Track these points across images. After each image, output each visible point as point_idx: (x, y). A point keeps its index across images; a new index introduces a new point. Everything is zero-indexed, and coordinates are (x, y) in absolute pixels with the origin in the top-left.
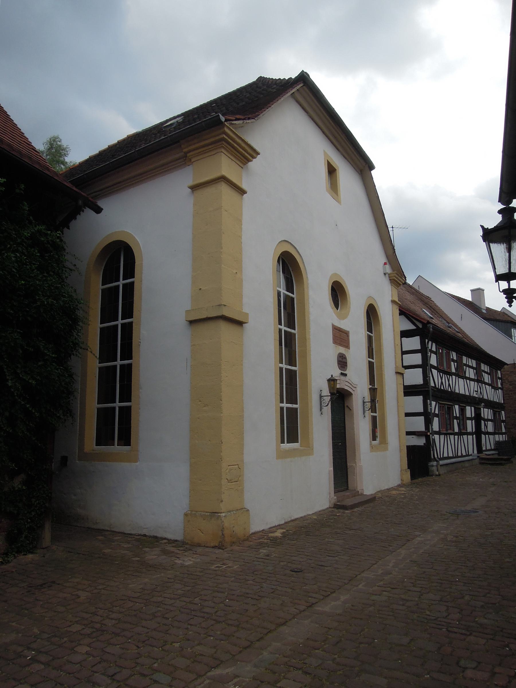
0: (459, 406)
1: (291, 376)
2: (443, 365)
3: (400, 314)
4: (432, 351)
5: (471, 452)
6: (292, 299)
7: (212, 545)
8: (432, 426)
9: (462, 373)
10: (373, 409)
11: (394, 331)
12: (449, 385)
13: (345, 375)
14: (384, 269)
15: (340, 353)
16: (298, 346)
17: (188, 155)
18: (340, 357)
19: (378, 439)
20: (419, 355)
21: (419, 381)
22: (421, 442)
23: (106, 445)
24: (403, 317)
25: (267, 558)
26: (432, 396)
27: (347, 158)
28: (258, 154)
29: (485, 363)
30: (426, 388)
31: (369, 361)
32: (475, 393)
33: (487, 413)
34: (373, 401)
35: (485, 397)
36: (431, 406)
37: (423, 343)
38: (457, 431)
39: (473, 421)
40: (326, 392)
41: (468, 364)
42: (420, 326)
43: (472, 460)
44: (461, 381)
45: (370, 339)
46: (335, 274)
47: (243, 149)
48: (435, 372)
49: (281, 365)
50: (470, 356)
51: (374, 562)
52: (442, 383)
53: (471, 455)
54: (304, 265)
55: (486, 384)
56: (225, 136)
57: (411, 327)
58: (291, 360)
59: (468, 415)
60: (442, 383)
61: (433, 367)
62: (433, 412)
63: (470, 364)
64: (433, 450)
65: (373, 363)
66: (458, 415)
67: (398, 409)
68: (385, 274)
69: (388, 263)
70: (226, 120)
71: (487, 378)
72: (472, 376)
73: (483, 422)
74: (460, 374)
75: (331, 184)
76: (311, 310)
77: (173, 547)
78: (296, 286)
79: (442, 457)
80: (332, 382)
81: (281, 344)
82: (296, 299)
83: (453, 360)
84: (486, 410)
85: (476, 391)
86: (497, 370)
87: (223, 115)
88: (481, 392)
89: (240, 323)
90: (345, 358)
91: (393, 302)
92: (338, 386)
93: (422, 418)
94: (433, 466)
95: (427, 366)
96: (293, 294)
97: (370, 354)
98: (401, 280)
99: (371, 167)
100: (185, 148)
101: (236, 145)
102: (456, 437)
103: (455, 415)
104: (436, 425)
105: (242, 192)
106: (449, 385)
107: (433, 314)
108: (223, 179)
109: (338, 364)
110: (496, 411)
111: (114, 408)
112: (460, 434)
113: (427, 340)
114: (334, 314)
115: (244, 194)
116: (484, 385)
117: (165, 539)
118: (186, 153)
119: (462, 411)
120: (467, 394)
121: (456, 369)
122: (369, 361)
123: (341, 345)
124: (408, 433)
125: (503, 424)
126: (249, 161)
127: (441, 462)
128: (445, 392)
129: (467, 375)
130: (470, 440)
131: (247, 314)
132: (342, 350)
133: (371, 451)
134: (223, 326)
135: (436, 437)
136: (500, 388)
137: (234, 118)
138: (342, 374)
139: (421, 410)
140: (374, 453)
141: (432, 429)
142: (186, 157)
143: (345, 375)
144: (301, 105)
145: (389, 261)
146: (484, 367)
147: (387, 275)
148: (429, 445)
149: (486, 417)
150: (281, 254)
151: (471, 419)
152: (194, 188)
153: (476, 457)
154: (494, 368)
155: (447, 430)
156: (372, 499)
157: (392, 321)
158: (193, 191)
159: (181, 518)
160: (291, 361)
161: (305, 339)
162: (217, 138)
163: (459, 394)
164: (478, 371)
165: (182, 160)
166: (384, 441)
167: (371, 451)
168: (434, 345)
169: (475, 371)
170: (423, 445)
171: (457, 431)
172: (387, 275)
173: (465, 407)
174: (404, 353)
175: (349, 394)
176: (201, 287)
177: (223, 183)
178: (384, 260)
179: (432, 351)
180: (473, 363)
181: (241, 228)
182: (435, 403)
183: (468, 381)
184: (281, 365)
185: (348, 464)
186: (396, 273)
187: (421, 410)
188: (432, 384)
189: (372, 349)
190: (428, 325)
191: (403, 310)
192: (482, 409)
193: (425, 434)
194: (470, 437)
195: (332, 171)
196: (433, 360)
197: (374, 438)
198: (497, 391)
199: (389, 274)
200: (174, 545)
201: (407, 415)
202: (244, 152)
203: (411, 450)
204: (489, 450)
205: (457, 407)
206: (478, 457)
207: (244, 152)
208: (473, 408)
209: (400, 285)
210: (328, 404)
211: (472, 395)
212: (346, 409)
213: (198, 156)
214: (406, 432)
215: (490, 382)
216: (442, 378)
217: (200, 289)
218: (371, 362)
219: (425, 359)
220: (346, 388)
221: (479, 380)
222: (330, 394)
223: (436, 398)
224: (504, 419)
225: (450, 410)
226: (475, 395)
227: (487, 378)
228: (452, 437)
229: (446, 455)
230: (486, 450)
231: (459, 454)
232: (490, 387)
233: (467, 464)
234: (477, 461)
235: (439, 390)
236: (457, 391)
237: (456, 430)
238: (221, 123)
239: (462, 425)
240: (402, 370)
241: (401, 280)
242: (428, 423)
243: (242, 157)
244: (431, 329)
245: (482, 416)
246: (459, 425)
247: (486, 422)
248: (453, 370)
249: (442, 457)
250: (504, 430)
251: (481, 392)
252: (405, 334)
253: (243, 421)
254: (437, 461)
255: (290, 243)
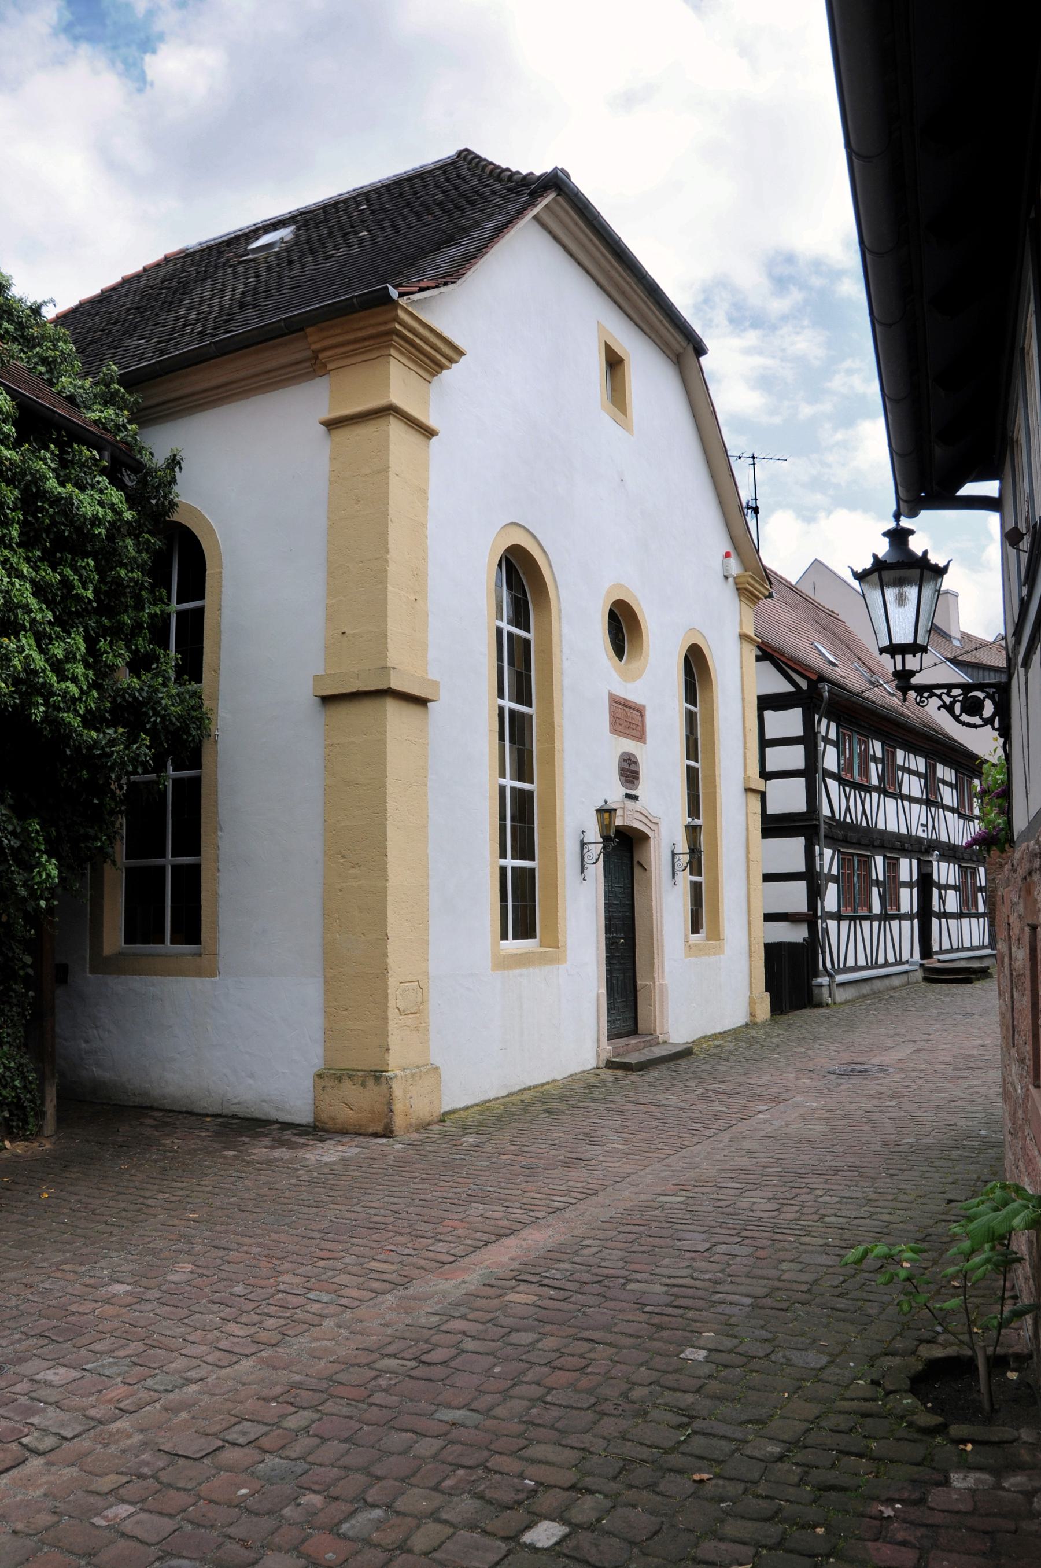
0: (885, 857)
1: (523, 804)
2: (851, 772)
3: (758, 659)
4: (826, 740)
5: (906, 956)
6: (527, 643)
7: (371, 1130)
8: (822, 901)
9: (893, 785)
10: (695, 865)
11: (743, 700)
12: (864, 812)
13: (635, 798)
14: (725, 566)
15: (625, 753)
16: (538, 741)
17: (321, 356)
18: (625, 760)
19: (703, 931)
20: (799, 750)
21: (800, 805)
22: (797, 934)
23: (146, 941)
24: (767, 665)
25: (476, 1149)
26: (825, 837)
27: (648, 331)
28: (461, 353)
29: (945, 764)
30: (813, 819)
31: (688, 767)
32: (920, 829)
33: (945, 872)
34: (694, 851)
35: (944, 838)
36: (822, 859)
37: (809, 724)
38: (879, 912)
39: (915, 890)
40: (593, 835)
41: (906, 765)
42: (804, 684)
43: (906, 972)
44: (891, 803)
45: (691, 717)
46: (619, 586)
47: (432, 347)
48: (833, 785)
49: (502, 781)
50: (911, 748)
51: (672, 1152)
52: (848, 809)
53: (907, 962)
54: (552, 572)
55: (945, 808)
56: (397, 326)
57: (787, 688)
58: (523, 769)
59: (904, 876)
60: (848, 809)
61: (828, 774)
62: (826, 871)
63: (913, 767)
64: (824, 953)
65: (697, 769)
66: (881, 878)
67: (748, 866)
68: (726, 577)
69: (733, 554)
70: (401, 295)
71: (948, 796)
72: (916, 793)
73: (935, 891)
74: (890, 788)
75: (613, 390)
76: (566, 664)
77: (295, 1134)
78: (535, 615)
79: (842, 966)
80: (606, 815)
81: (501, 737)
82: (538, 717)
83: (875, 759)
84: (944, 865)
85: (922, 825)
86: (972, 778)
87: (395, 287)
88: (934, 827)
89: (421, 702)
90: (636, 763)
91: (743, 637)
92: (619, 822)
93: (802, 886)
94: (821, 986)
95: (816, 771)
96: (528, 631)
97: (692, 751)
98: (762, 589)
99: (700, 350)
100: (315, 343)
101: (418, 341)
102: (876, 924)
103: (874, 877)
104: (831, 900)
105: (428, 433)
106: (864, 812)
107: (839, 653)
108: (390, 410)
109: (621, 775)
110: (967, 868)
111: (163, 868)
112: (885, 917)
113: (817, 717)
114: (614, 673)
115: (433, 435)
116: (941, 811)
117: (277, 1122)
118: (316, 353)
119: (892, 866)
120: (904, 831)
121: (881, 779)
122: (688, 767)
123: (627, 735)
124: (769, 917)
125: (979, 895)
126: (442, 367)
127: (840, 978)
128: (853, 827)
129: (905, 791)
130: (906, 931)
131: (435, 684)
132: (629, 745)
133: (686, 956)
134: (392, 707)
135: (832, 924)
136: (978, 818)
137: (416, 289)
138: (628, 796)
139: (801, 867)
140: (693, 959)
141: (823, 908)
142: (317, 358)
143: (635, 798)
144: (550, 232)
145: (736, 548)
146: (944, 772)
147: (731, 580)
148: (814, 944)
149: (943, 881)
150: (507, 550)
151: (909, 885)
152: (332, 425)
153: (917, 967)
154: (964, 774)
155: (855, 911)
156: (685, 1053)
157: (738, 679)
158: (329, 430)
159: (308, 1083)
160: (523, 771)
161: (552, 725)
162: (383, 328)
163: (885, 832)
164: (930, 781)
165: (308, 364)
166: (715, 935)
167: (686, 956)
168: (833, 726)
169: (922, 781)
170: (801, 941)
171: (879, 912)
172: (731, 580)
173: (898, 859)
174: (764, 743)
175: (644, 838)
176: (344, 630)
177: (392, 419)
178: (726, 546)
179: (826, 740)
180: (919, 763)
181: (426, 507)
182: (831, 851)
183: (906, 803)
184: (502, 781)
185: (639, 982)
186: (751, 576)
187: (801, 867)
188: (826, 811)
189: (696, 740)
190: (820, 686)
191: (769, 650)
192: (935, 863)
193: (811, 918)
194: (906, 924)
195: (614, 363)
196: (830, 760)
197: (696, 928)
198: (971, 824)
199: (735, 578)
200: (295, 1132)
201: (768, 878)
202: (433, 353)
203: (773, 952)
204: (951, 950)
205: (879, 860)
206: (921, 965)
207: (433, 353)
208: (915, 862)
209: (759, 598)
210: (597, 860)
211: (914, 834)
212: (637, 870)
213: (342, 358)
214: (765, 915)
215: (955, 806)
216: (847, 799)
217: (344, 633)
218: (693, 768)
219: (813, 757)
220: (637, 825)
221: (931, 802)
222: (601, 840)
223: (833, 841)
224: (983, 884)
225: (866, 863)
226: (921, 834)
227: (948, 796)
228: (866, 924)
229: (850, 963)
230: (941, 952)
231: (881, 961)
232: (956, 815)
233: (896, 981)
234: (919, 974)
235: (842, 825)
236: (881, 826)
237: (877, 909)
238: (389, 300)
239: (890, 898)
240: (759, 784)
241: (762, 589)
242: (815, 894)
243: (428, 362)
244: (826, 694)
245: (935, 877)
246: (882, 898)
247: (943, 892)
248: (875, 781)
249: (842, 966)
250: (981, 909)
251: (934, 827)
252: (767, 703)
253: (428, 895)
254: (830, 975)
255: (524, 528)
